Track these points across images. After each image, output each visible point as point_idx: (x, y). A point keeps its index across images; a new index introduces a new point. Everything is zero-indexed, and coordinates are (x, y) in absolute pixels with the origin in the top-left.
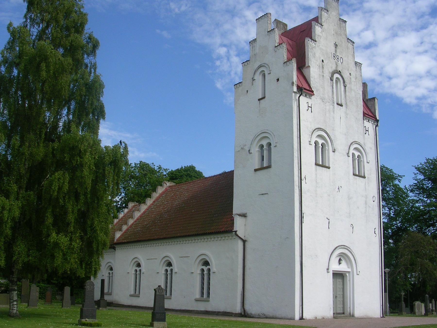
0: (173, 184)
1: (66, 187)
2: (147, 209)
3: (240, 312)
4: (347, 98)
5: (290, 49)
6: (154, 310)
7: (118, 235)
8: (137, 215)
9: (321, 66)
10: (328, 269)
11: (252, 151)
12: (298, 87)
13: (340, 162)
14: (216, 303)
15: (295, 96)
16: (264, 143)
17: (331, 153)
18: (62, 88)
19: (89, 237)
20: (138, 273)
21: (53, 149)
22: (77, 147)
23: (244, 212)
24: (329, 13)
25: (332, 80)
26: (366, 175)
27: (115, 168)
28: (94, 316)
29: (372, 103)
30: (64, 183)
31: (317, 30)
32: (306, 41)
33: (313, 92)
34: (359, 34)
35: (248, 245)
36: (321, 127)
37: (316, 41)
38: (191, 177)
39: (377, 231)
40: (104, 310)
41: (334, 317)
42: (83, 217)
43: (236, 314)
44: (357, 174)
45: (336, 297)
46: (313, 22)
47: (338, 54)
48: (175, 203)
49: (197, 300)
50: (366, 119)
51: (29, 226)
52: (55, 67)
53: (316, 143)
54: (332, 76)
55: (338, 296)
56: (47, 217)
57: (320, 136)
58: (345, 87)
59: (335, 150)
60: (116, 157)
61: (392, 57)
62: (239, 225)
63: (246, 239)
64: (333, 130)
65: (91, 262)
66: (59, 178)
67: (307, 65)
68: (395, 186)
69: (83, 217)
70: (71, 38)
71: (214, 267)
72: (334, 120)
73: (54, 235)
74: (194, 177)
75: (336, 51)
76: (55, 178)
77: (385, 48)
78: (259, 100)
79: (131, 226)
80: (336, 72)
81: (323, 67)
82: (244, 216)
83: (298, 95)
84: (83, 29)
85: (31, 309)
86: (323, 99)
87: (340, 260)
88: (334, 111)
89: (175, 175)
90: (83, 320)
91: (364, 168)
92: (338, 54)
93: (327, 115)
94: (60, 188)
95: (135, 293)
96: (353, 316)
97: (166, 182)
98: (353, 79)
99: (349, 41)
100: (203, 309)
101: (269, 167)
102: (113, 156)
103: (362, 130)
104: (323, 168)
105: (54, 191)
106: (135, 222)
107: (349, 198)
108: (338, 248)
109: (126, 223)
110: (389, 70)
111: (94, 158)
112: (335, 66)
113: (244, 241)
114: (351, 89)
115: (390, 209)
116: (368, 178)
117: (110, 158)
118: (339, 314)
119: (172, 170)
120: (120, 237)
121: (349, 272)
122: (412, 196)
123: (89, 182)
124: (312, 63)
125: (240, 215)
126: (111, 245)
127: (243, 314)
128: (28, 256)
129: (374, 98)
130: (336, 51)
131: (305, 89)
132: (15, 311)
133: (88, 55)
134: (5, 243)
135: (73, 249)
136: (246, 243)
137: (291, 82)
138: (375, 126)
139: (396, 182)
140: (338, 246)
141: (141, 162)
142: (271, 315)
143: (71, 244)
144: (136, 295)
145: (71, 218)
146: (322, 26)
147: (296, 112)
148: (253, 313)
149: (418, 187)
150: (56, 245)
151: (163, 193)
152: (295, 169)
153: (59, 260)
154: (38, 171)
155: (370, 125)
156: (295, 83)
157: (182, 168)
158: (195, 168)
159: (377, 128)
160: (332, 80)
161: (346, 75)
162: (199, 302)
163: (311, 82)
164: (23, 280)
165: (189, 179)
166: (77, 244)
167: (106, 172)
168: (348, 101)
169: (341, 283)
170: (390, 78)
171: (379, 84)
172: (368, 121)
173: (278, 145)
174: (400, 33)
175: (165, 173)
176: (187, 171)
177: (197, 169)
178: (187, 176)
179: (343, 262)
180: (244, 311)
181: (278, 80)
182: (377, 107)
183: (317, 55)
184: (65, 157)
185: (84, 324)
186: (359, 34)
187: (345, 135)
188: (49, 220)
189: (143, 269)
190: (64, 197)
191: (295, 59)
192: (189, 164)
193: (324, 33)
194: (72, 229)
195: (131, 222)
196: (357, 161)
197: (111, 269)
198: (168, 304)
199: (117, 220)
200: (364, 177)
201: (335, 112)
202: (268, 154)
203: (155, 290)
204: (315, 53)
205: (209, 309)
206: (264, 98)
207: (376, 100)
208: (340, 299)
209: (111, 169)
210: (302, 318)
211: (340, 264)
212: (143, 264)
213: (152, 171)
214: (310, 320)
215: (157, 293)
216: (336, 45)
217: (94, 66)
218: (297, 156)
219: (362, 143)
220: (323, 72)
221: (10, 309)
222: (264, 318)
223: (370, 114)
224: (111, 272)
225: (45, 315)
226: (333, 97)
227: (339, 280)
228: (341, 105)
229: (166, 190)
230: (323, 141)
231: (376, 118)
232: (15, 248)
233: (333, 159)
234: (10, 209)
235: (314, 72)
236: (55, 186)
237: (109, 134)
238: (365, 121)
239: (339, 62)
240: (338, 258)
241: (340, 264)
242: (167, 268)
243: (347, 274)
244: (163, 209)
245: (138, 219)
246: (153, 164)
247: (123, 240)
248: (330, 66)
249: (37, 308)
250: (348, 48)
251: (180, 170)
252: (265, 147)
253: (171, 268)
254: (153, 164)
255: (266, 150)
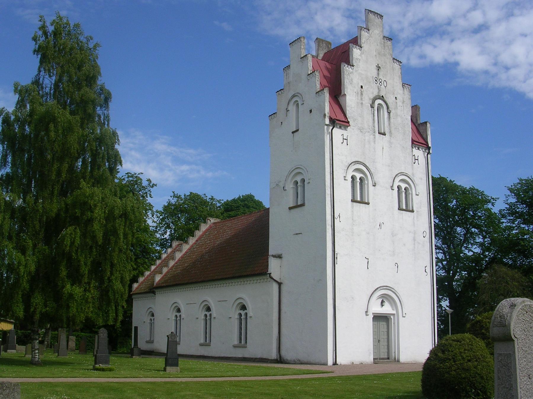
0: (218, 220)
1: (78, 241)
2: (189, 249)
3: (276, 358)
4: (392, 125)
5: (327, 74)
6: (167, 356)
7: (158, 278)
8: (178, 255)
9: (359, 93)
10: (367, 312)
11: (286, 188)
12: (331, 119)
13: (383, 197)
14: (253, 350)
15: (328, 130)
16: (299, 179)
17: (371, 188)
18: (71, 147)
19: (107, 286)
20: (208, 317)
21: (66, 205)
22: (87, 202)
23: (279, 252)
24: (370, 32)
25: (372, 107)
26: (414, 209)
27: (126, 220)
28: (107, 362)
29: (424, 128)
30: (75, 238)
31: (356, 52)
32: (342, 66)
33: (348, 122)
34: (464, 16)
35: (283, 288)
36: (359, 160)
37: (353, 66)
38: (248, 207)
39: (428, 270)
40: (138, 357)
41: (375, 363)
42: (97, 268)
43: (271, 360)
44: (404, 208)
45: (379, 341)
46: (350, 44)
47: (381, 77)
48: (217, 242)
49: (235, 347)
50: (415, 147)
51: (46, 278)
52: (63, 130)
53: (353, 178)
54: (373, 102)
55: (382, 340)
56: (61, 269)
57: (357, 170)
58: (389, 113)
59: (375, 184)
60: (126, 209)
61: (508, 43)
62: (274, 267)
63: (282, 281)
64: (374, 162)
65: (108, 311)
66: (71, 234)
67: (342, 94)
68: (489, 210)
69: (97, 268)
70: (82, 92)
71: (250, 312)
72: (375, 151)
73: (68, 286)
74: (253, 207)
75: (378, 74)
76: (67, 234)
77: (499, 31)
78: (293, 132)
79: (171, 269)
80: (378, 97)
81: (362, 94)
82: (279, 257)
83: (331, 128)
84: (95, 82)
85: (61, 358)
86: (361, 130)
87: (382, 302)
88: (375, 141)
89: (231, 206)
90: (97, 366)
91: (412, 201)
92: (381, 77)
93: (367, 146)
94: (72, 243)
95: (240, 342)
96: (398, 361)
97: (210, 218)
98: (399, 103)
99: (395, 61)
100: (240, 356)
101: (303, 205)
102: (123, 208)
103: (410, 159)
104: (361, 204)
105: (66, 246)
106: (176, 263)
107: (393, 235)
108: (379, 289)
109: (167, 266)
110: (505, 58)
111: (105, 212)
112: (377, 90)
113: (280, 284)
114: (397, 115)
115: (484, 237)
116: (417, 212)
117: (120, 212)
118: (383, 359)
119: (227, 201)
120: (160, 281)
121: (394, 315)
122: (505, 223)
123: (100, 236)
124: (349, 90)
125: (274, 256)
126: (151, 289)
127: (279, 359)
128: (46, 306)
129: (426, 123)
130: (378, 74)
131: (340, 120)
132: (37, 359)
133: (101, 106)
134: (23, 295)
135: (87, 299)
136: (282, 286)
137: (323, 114)
138: (426, 154)
139: (490, 206)
140: (378, 288)
141: (191, 193)
142: (305, 360)
143: (85, 294)
144: (206, 344)
145: (85, 270)
146: (361, 47)
147: (329, 148)
148: (289, 359)
149: (512, 211)
150: (71, 296)
151: (207, 230)
152: (327, 207)
153: (73, 310)
154: (52, 228)
155: (420, 153)
156: (327, 115)
157: (240, 197)
158: (254, 197)
159: (429, 156)
160: (372, 107)
161: (390, 100)
162: (237, 349)
163: (347, 112)
164: (60, 329)
165: (247, 210)
166: (94, 293)
167: (117, 225)
168: (393, 129)
169: (386, 326)
170: (507, 68)
171: (494, 76)
172: (418, 149)
173: (311, 181)
174: (516, 12)
175: (218, 205)
176: (244, 201)
177: (256, 198)
178: (244, 207)
179: (386, 304)
180: (280, 357)
181: (311, 111)
182: (429, 133)
183: (355, 81)
184: (76, 213)
185: (97, 369)
186: (464, 16)
187: (389, 166)
188: (64, 273)
189: (183, 314)
190: (77, 251)
191: (327, 88)
192: (248, 193)
193: (363, 56)
194: (86, 280)
195: (172, 263)
196: (404, 194)
197: (153, 315)
198: (181, 350)
199: (160, 261)
200: (412, 211)
201: (376, 142)
202: (305, 189)
203: (167, 336)
204: (352, 79)
205: (247, 356)
206: (297, 131)
207: (428, 125)
208: (384, 343)
209: (121, 221)
210: (335, 364)
211: (382, 306)
212: (182, 309)
213: (204, 203)
214: (345, 366)
215: (170, 339)
216: (379, 68)
217: (107, 118)
218: (329, 193)
219: (410, 174)
220: (362, 99)
221: (32, 357)
222: (299, 364)
223: (421, 141)
224: (152, 318)
225: (69, 363)
226: (374, 126)
227: (383, 324)
228: (384, 134)
229: (210, 227)
230: (362, 175)
231: (427, 145)
232: (32, 300)
233: (372, 193)
234: (26, 264)
235: (351, 99)
236: (67, 242)
237: (169, 150)
238: (414, 149)
239: (383, 86)
240: (380, 300)
241: (382, 306)
242: (207, 313)
243: (392, 317)
244: (205, 249)
245: (179, 260)
246: (205, 195)
247: (163, 283)
248: (371, 92)
249: (67, 357)
250: (393, 69)
251: (237, 200)
252: (299, 184)
253: (245, 311)
254: (205, 195)
255: (300, 186)
